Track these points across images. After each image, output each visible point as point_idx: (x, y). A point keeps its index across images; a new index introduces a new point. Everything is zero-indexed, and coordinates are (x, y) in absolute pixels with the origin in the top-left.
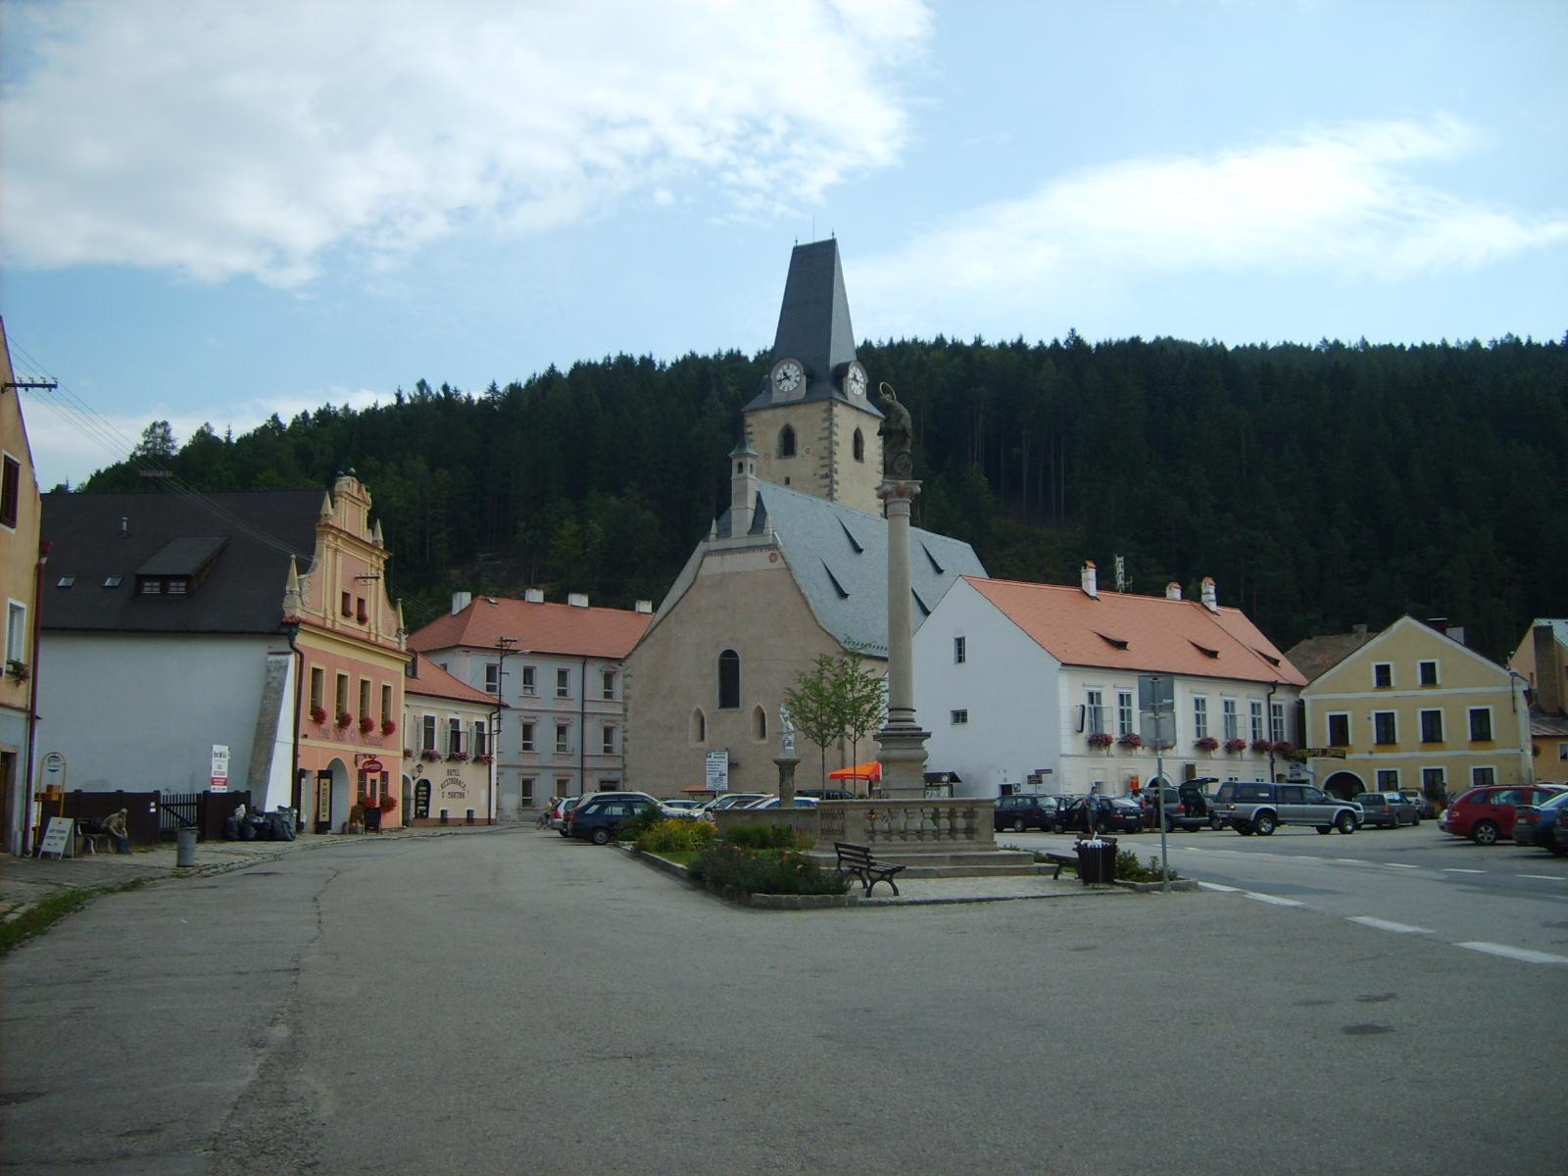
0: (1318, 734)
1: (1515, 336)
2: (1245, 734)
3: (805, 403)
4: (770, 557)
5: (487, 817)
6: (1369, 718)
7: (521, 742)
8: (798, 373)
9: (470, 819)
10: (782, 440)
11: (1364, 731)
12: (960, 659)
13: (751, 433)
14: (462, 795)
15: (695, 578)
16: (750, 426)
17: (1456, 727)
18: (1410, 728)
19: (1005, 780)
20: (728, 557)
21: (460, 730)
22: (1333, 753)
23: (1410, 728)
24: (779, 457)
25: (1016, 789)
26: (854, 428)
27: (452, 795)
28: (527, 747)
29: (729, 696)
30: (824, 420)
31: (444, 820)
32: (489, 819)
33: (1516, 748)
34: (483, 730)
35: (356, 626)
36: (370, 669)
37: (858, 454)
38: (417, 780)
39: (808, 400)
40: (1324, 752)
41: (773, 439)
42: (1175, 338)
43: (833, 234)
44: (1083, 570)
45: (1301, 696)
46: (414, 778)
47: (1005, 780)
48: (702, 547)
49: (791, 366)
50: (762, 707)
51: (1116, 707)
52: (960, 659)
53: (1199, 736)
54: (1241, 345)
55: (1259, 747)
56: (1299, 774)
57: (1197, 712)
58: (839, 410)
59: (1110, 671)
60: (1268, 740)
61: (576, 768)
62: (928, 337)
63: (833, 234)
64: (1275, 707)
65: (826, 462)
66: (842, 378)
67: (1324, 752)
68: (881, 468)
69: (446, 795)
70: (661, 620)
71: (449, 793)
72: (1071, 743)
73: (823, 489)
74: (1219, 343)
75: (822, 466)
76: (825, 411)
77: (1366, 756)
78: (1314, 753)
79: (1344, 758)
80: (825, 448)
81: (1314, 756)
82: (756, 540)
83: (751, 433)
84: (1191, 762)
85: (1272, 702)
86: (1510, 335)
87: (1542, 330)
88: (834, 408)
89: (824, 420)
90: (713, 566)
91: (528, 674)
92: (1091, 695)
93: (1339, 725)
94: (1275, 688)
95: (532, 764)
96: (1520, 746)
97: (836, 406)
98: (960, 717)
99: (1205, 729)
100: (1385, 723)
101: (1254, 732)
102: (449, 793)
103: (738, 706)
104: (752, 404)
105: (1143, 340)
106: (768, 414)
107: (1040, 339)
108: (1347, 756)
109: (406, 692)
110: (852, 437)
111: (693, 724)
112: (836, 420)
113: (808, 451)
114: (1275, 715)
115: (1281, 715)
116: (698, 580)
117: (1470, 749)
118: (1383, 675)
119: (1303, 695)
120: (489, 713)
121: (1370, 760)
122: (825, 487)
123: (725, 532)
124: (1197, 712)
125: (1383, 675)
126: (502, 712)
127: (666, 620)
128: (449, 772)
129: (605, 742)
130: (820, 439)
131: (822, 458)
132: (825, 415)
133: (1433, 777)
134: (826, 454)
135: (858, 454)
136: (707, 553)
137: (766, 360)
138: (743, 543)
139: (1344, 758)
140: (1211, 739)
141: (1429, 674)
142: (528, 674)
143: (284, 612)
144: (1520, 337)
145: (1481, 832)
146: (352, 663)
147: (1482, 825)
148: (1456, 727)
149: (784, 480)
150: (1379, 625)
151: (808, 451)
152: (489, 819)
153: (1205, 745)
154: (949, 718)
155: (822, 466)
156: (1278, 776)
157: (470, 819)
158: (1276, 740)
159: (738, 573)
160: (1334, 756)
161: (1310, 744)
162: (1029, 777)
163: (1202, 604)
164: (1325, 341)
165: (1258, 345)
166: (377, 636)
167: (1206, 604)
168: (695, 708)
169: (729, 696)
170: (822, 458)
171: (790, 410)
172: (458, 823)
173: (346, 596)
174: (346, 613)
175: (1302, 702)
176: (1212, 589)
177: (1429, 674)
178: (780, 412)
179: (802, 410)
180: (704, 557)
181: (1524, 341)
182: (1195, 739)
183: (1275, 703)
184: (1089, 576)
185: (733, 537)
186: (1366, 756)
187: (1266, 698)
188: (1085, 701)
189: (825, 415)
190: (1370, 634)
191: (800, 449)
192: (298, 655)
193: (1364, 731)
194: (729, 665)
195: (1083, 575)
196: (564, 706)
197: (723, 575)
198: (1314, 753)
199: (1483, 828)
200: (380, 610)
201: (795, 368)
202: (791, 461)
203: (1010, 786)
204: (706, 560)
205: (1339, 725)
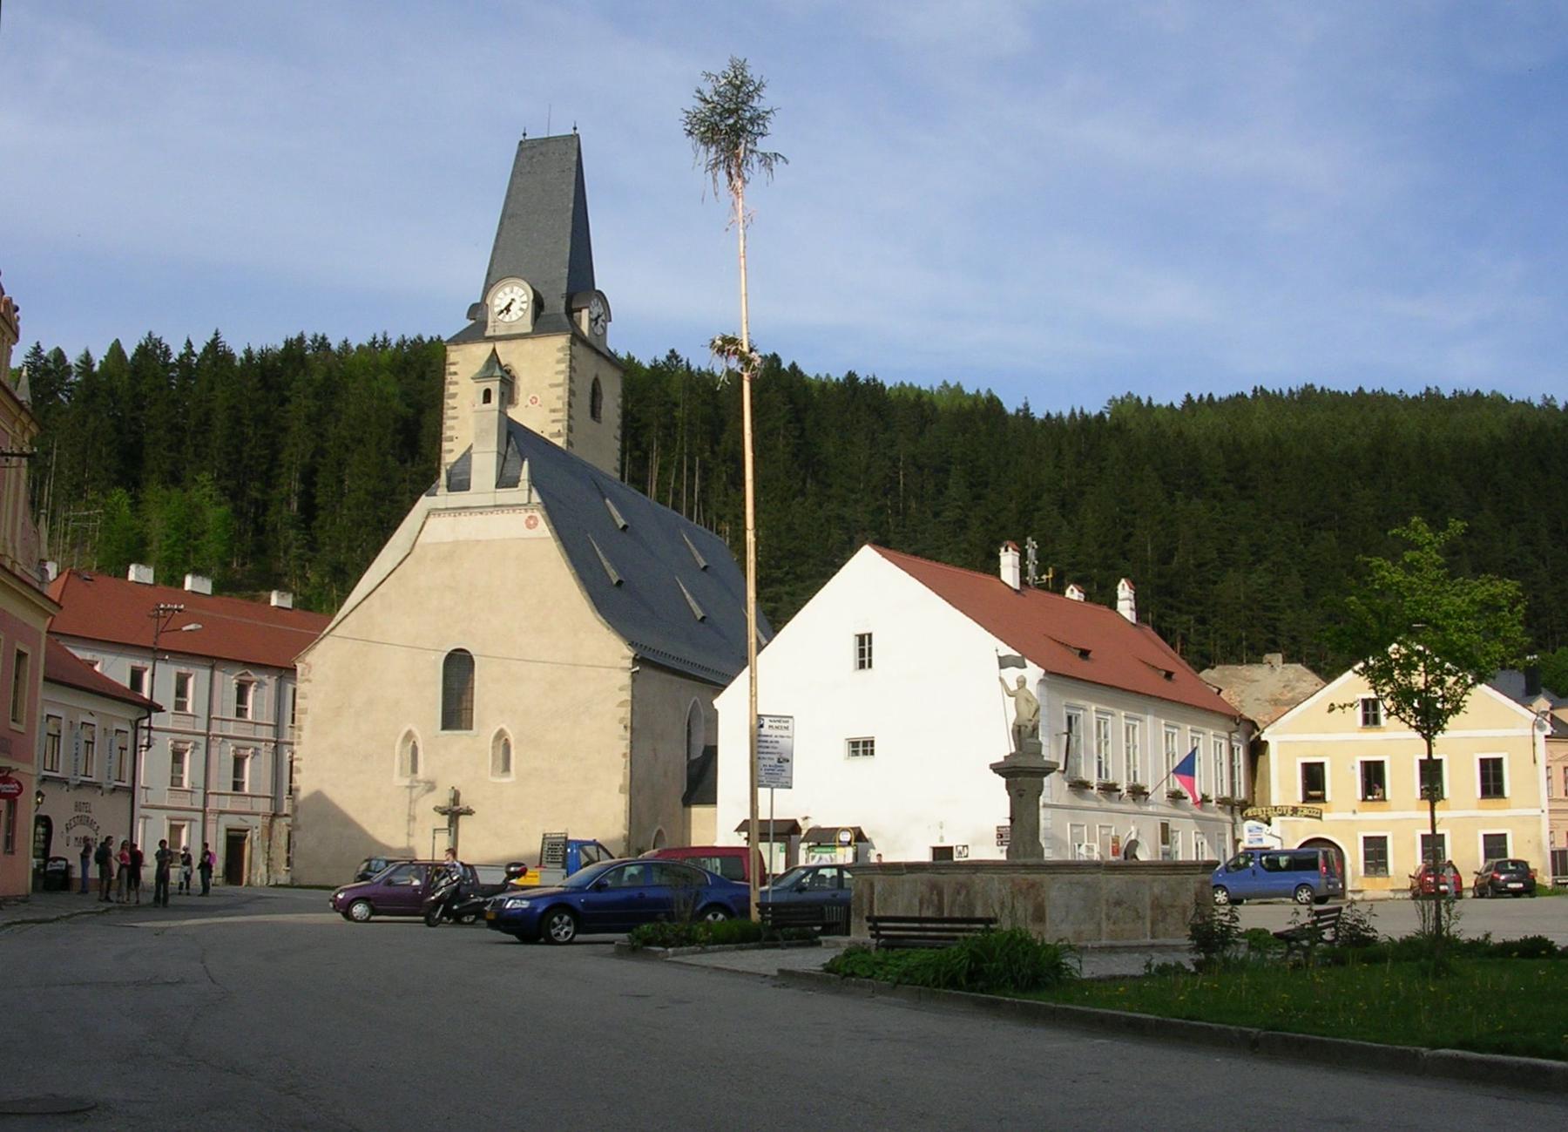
1: (1136, 395)
4: (527, 522)
6: (1353, 768)
11: (1343, 783)
19: (942, 839)
20: (465, 519)
22: (1306, 812)
29: (456, 712)
33: (1537, 807)
40: (1295, 811)
43: (575, 129)
48: (424, 502)
49: (516, 289)
50: (508, 731)
56: (1261, 840)
61: (197, 810)
63: (575, 129)
67: (1295, 811)
68: (619, 433)
69: (72, 842)
75: (554, 421)
77: (1350, 816)
79: (1320, 818)
81: (1282, 815)
82: (507, 496)
86: (1130, 395)
93: (1313, 777)
96: (1540, 807)
98: (862, 747)
103: (471, 729)
107: (671, 348)
108: (1325, 816)
111: (399, 753)
113: (534, 401)
116: (417, 549)
117: (1479, 808)
120: (134, 718)
121: (1353, 821)
126: (154, 715)
128: (78, 806)
130: (552, 386)
131: (553, 411)
133: (1495, 845)
138: (488, 500)
139: (1320, 818)
144: (1141, 397)
145: (561, 919)
147: (708, 914)
151: (534, 401)
154: (844, 748)
155: (554, 421)
159: (478, 541)
160: (1307, 816)
164: (946, 385)
166: (13, 562)
169: (456, 712)
170: (553, 411)
179: (528, 344)
180: (427, 517)
181: (1145, 402)
186: (1350, 816)
190: (1285, 665)
193: (1343, 783)
194: (459, 666)
197: (456, 543)
199: (556, 919)
200: (20, 513)
201: (522, 292)
204: (432, 521)
205: (1313, 777)
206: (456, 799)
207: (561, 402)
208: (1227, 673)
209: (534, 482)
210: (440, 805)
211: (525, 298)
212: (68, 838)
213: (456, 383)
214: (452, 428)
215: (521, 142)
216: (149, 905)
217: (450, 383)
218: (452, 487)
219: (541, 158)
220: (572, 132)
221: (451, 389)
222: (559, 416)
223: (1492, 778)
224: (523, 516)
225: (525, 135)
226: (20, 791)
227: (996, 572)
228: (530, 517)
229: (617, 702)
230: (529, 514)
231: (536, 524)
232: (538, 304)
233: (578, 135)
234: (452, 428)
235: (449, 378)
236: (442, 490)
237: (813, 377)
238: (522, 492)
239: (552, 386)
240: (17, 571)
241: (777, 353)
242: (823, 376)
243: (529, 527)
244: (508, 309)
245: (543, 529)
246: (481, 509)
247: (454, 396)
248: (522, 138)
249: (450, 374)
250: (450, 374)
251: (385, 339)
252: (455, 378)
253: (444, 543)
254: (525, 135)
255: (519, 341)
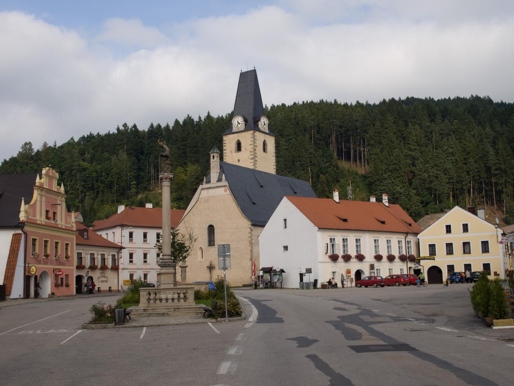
0: (425, 252)
2: (395, 252)
3: (244, 132)
5: (117, 289)
7: (143, 260)
8: (242, 120)
9: (110, 290)
10: (237, 145)
11: (441, 250)
12: (286, 227)
13: (225, 143)
14: (107, 281)
15: (199, 198)
16: (225, 141)
17: (476, 247)
18: (458, 248)
19: (301, 272)
20: (210, 190)
21: (95, 257)
23: (458, 248)
24: (236, 152)
25: (304, 275)
26: (263, 140)
27: (102, 281)
28: (145, 262)
30: (252, 138)
31: (99, 290)
32: (118, 290)
34: (115, 257)
35: (53, 222)
36: (59, 237)
37: (265, 150)
38: (87, 277)
39: (246, 130)
41: (234, 146)
42: (415, 97)
43: (254, 68)
44: (334, 192)
45: (418, 237)
46: (86, 276)
47: (301, 272)
48: (201, 187)
49: (239, 118)
51: (354, 244)
52: (286, 227)
53: (400, 254)
54: (440, 99)
55: (403, 258)
57: (357, 244)
58: (257, 134)
59: (338, 230)
60: (405, 254)
62: (316, 100)
63: (254, 68)
64: (408, 242)
65: (252, 153)
66: (258, 122)
69: (100, 281)
70: (187, 214)
71: (101, 281)
72: (322, 257)
73: (251, 163)
74: (431, 98)
75: (251, 155)
76: (251, 134)
78: (424, 259)
80: (252, 148)
82: (220, 184)
83: (225, 143)
84: (372, 263)
85: (406, 240)
87: (509, 100)
88: (255, 133)
89: (252, 138)
90: (204, 193)
91: (131, 235)
92: (331, 239)
93: (432, 247)
94: (407, 235)
95: (147, 268)
97: (256, 132)
99: (347, 250)
100: (466, 245)
101: (400, 252)
102: (101, 281)
104: (224, 133)
105: (376, 104)
106: (231, 136)
107: (357, 100)
109: (77, 244)
110: (262, 144)
112: (256, 138)
113: (246, 149)
114: (408, 244)
115: (411, 244)
116: (199, 199)
118: (448, 229)
119: (419, 236)
122: (252, 162)
123: (209, 182)
124: (357, 244)
125: (448, 229)
127: (189, 214)
129: (144, 259)
130: (250, 145)
131: (251, 152)
132: (252, 136)
134: (252, 150)
135: (265, 150)
136: (203, 189)
137: (231, 116)
140: (349, 255)
141: (465, 228)
142: (131, 235)
143: (20, 219)
146: (51, 236)
148: (476, 247)
149: (237, 160)
150: (443, 211)
152: (118, 290)
153: (379, 258)
155: (251, 155)
156: (409, 268)
157: (110, 290)
158: (409, 254)
159: (214, 196)
161: (422, 255)
162: (496, 272)
163: (383, 203)
165: (447, 98)
167: (384, 203)
168: (200, 246)
170: (251, 152)
171: (239, 134)
172: (105, 291)
173: (47, 212)
174: (47, 218)
175: (418, 239)
176: (386, 198)
177: (465, 228)
178: (236, 135)
179: (243, 134)
180: (201, 191)
182: (374, 254)
183: (408, 240)
184: (336, 196)
185: (211, 183)
187: (404, 239)
188: (329, 242)
189: (252, 136)
191: (243, 149)
192: (25, 234)
193: (441, 250)
194: (211, 229)
195: (334, 194)
196: (145, 246)
198: (424, 259)
201: (241, 119)
202: (240, 153)
203: (302, 274)
205: (432, 247)
206: (211, 264)
207: (252, 149)
208: (433, 216)
209: (226, 180)
210: (208, 266)
211: (242, 120)
212: (99, 281)
213: (226, 146)
214: (226, 159)
215: (241, 73)
216: (33, 298)
217: (224, 146)
218: (207, 183)
219: (246, 77)
220: (254, 69)
221: (225, 148)
222: (252, 153)
223: (485, 247)
224: (223, 189)
225: (241, 71)
226: (63, 274)
227: (332, 198)
228: (225, 189)
229: (248, 236)
230: (225, 188)
231: (227, 191)
232: (246, 121)
233: (255, 70)
234: (226, 159)
235: (224, 145)
236: (204, 183)
237: (424, 99)
238: (224, 183)
239: (250, 145)
240: (63, 227)
241: (394, 97)
242: (428, 97)
243: (225, 192)
244: (265, 124)
245: (228, 192)
246: (214, 188)
247: (225, 150)
248: (241, 72)
249: (224, 143)
250: (224, 143)
251: (266, 107)
252: (225, 145)
253: (206, 197)
254: (241, 71)
255: (241, 133)
